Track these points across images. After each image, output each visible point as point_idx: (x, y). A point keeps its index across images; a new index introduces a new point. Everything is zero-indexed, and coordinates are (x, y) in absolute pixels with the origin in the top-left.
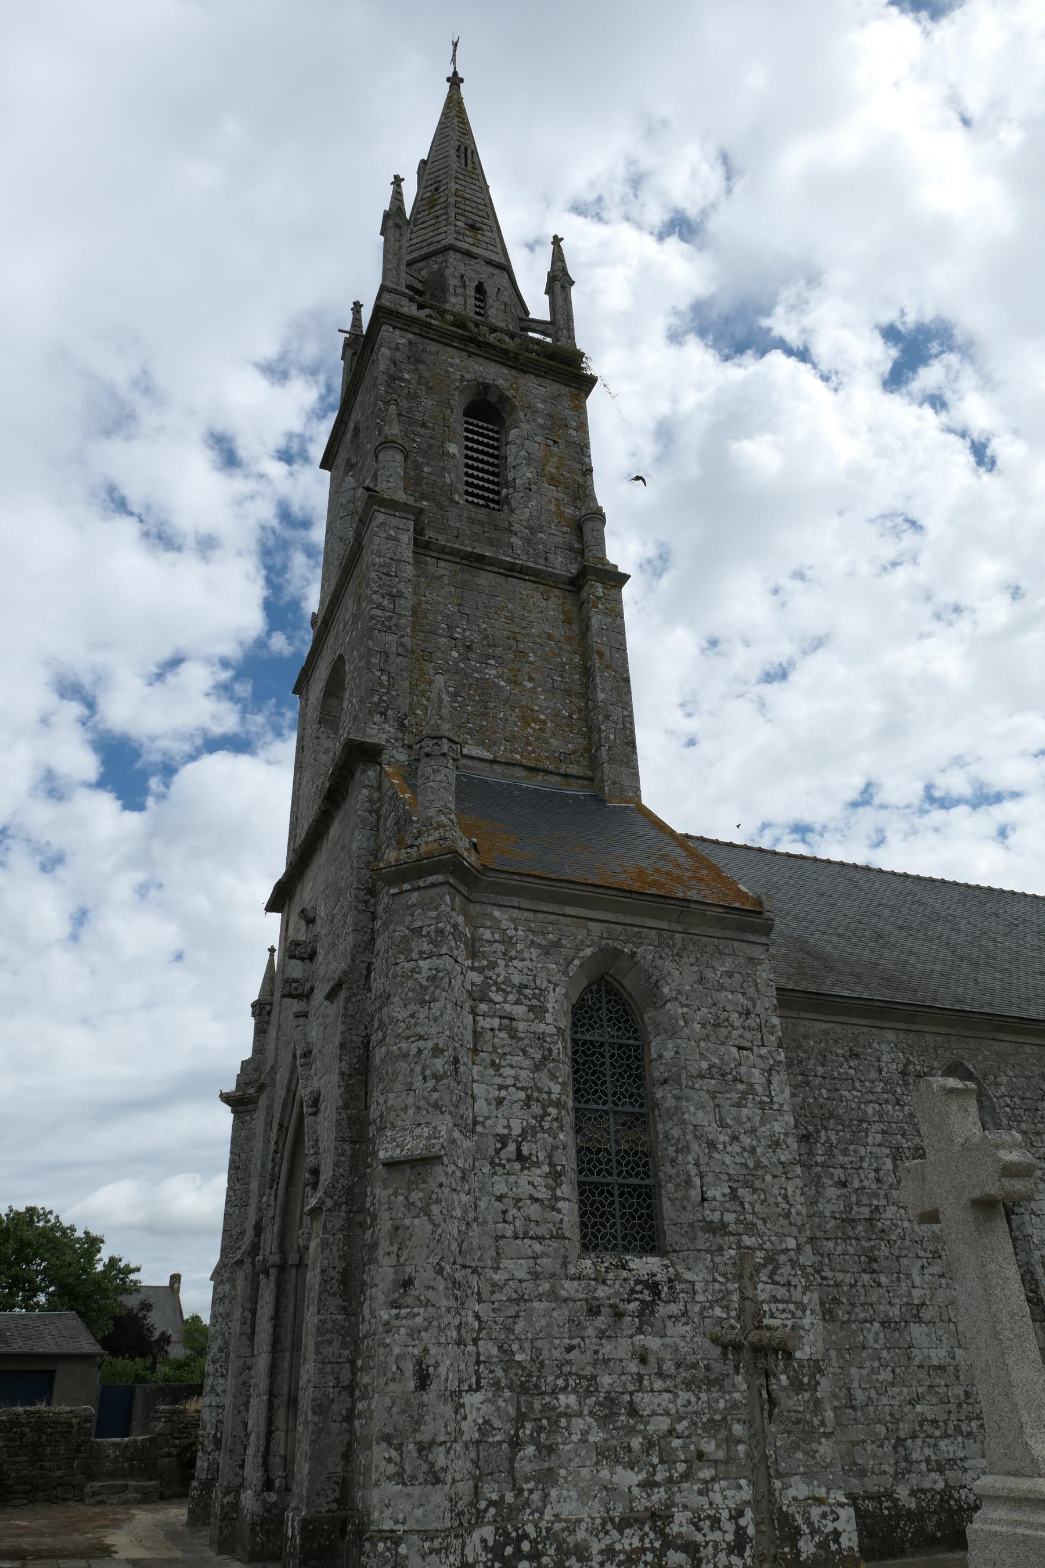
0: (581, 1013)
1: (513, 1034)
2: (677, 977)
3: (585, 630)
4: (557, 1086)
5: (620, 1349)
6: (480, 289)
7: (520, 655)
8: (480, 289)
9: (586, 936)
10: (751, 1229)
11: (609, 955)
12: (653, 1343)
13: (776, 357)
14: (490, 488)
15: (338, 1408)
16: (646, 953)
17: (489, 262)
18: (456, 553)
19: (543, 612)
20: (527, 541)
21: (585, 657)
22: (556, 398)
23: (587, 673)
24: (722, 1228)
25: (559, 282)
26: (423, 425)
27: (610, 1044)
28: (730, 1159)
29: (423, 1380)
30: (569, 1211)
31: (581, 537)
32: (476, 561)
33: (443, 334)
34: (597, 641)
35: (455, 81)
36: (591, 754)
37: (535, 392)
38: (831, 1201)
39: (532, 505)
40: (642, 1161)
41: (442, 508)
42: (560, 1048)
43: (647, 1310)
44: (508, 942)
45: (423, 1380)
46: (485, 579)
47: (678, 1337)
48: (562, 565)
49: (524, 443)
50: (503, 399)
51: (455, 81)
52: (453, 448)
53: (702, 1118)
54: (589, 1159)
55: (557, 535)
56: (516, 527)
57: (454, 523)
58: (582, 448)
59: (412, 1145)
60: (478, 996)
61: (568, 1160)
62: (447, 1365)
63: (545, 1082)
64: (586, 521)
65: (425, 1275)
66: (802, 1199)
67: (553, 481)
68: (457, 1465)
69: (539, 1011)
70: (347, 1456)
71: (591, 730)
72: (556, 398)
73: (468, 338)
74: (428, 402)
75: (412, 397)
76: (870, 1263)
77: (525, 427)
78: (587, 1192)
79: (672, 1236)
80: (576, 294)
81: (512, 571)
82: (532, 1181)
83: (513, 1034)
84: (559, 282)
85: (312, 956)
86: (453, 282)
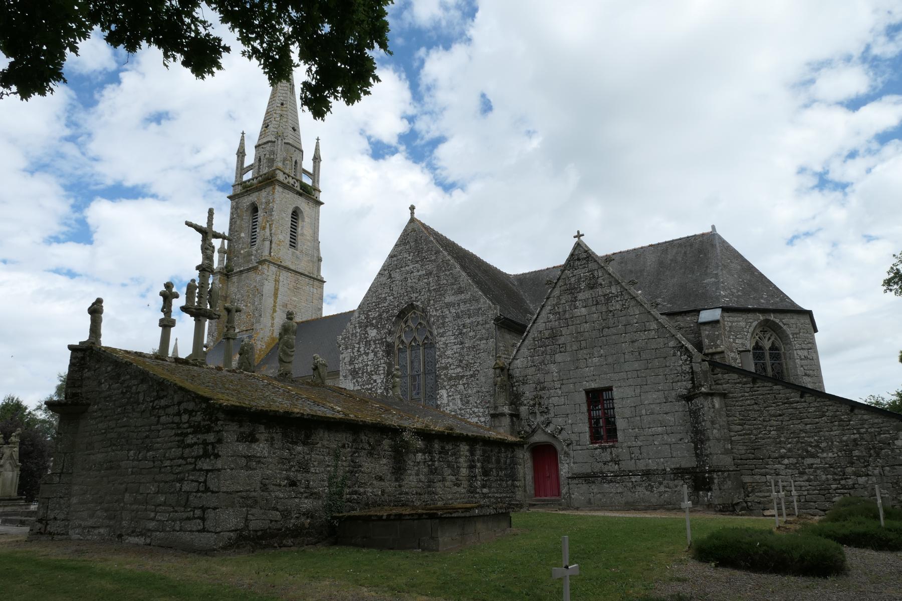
25: (317, 159)
84: (317, 159)
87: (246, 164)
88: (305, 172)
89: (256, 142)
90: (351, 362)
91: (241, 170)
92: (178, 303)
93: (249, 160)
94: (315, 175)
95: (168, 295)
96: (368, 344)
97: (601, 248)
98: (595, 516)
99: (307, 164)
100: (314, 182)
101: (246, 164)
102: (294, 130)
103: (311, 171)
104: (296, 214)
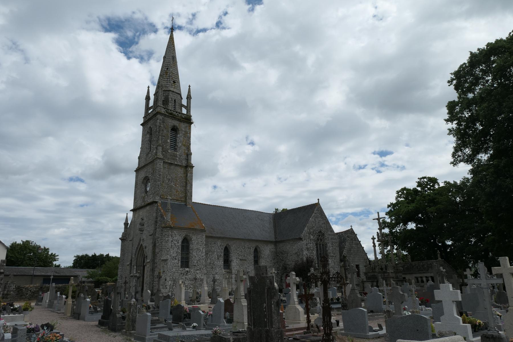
0: (183, 242)
2: (194, 238)
3: (187, 176)
4: (180, 251)
5: (184, 277)
6: (175, 100)
7: (177, 180)
8: (175, 100)
11: (187, 235)
14: (174, 147)
15: (152, 283)
16: (191, 235)
17: (177, 93)
19: (180, 172)
20: (179, 158)
21: (186, 181)
22: (186, 127)
23: (186, 183)
24: (195, 266)
25: (189, 97)
27: (186, 244)
28: (197, 258)
29: (166, 280)
30: (180, 264)
31: (188, 157)
32: (171, 164)
33: (168, 116)
34: (189, 179)
36: (186, 197)
37: (182, 126)
38: (209, 261)
40: (188, 258)
42: (180, 247)
43: (187, 274)
45: (166, 280)
46: (172, 167)
47: (189, 276)
48: (184, 163)
49: (180, 137)
50: (177, 128)
52: (169, 141)
54: (182, 258)
55: (184, 156)
57: (168, 156)
58: (189, 138)
59: (165, 258)
60: (172, 241)
61: (180, 259)
62: (168, 279)
64: (189, 155)
66: (171, 317)
67: (184, 146)
68: (168, 287)
69: (178, 243)
70: (153, 288)
71: (186, 193)
72: (186, 127)
73: (172, 116)
74: (165, 131)
75: (163, 130)
76: (212, 268)
78: (182, 262)
79: (190, 266)
80: (192, 101)
81: (177, 165)
82: (176, 261)
84: (189, 97)
85: (143, 225)
86: (170, 99)
87: (150, 106)
88: (184, 106)
89: (154, 93)
90: (306, 245)
91: (147, 108)
92: (376, 240)
93: (151, 104)
94: (188, 108)
95: (373, 239)
96: (310, 240)
97: (121, 237)
98: (453, 310)
99: (184, 102)
100: (187, 112)
101: (150, 106)
102: (174, 82)
103: (186, 105)
104: (175, 129)
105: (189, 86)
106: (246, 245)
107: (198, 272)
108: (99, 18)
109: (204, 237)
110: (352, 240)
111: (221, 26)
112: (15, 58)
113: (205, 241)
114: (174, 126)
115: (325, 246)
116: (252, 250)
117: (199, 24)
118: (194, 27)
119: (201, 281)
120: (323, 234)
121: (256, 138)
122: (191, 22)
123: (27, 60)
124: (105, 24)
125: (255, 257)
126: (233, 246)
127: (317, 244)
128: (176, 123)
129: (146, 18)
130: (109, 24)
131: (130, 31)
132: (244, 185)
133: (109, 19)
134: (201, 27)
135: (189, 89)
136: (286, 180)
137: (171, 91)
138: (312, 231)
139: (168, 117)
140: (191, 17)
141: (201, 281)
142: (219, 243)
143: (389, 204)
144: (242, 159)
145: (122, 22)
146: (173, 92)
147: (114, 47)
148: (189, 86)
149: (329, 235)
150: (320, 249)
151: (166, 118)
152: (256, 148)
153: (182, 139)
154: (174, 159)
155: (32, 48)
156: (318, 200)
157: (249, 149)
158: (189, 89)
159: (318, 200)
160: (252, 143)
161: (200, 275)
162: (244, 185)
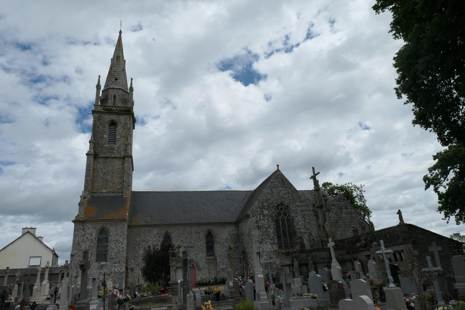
1: (88, 239)
6: (115, 96)
7: (114, 173)
8: (115, 96)
9: (99, 226)
10: (117, 258)
12: (102, 271)
13: (20, 234)
14: (113, 140)
16: (108, 226)
18: (103, 157)
20: (117, 151)
22: (126, 119)
26: (100, 133)
32: (107, 158)
33: (104, 112)
35: (120, 32)
37: (122, 119)
39: (120, 141)
41: (102, 148)
43: (101, 268)
44: (88, 228)
46: (108, 160)
50: (116, 122)
51: (120, 32)
53: (113, 246)
55: (123, 148)
56: (115, 148)
63: (91, 244)
65: (73, 267)
66: (184, 249)
67: (123, 137)
69: (92, 236)
72: (126, 119)
74: (101, 127)
75: (98, 127)
77: (119, 127)
83: (88, 239)
86: (109, 96)
90: (256, 223)
96: (264, 216)
105: (99, 76)
106: (193, 230)
107: (116, 265)
108: (215, 63)
109: (126, 226)
110: (340, 208)
111: (310, 37)
112: (168, 109)
113: (128, 231)
114: (113, 120)
115: (290, 221)
116: (203, 235)
117: (292, 42)
118: (289, 46)
119: (120, 274)
120: (287, 206)
121: (368, 124)
122: (286, 44)
123: (175, 108)
124: (220, 67)
125: (207, 243)
126: (215, 230)
127: (277, 220)
128: (114, 117)
129: (250, 52)
130: (224, 66)
131: (240, 65)
132: (369, 167)
133: (222, 62)
134: (295, 44)
135: (99, 80)
136: (412, 155)
137: (110, 88)
138: (265, 204)
139: (104, 113)
140: (285, 39)
141: (120, 274)
142: (155, 231)
143: (435, 154)
144: (360, 145)
145: (231, 61)
146: (113, 88)
147: (231, 80)
148: (99, 76)
149: (298, 206)
150: (284, 225)
151: (103, 115)
152: (373, 131)
153: (120, 131)
154: (111, 153)
155: (176, 100)
156: (278, 166)
157: (365, 134)
158: (99, 80)
159: (278, 166)
160: (367, 128)
161: (119, 268)
162: (369, 167)
